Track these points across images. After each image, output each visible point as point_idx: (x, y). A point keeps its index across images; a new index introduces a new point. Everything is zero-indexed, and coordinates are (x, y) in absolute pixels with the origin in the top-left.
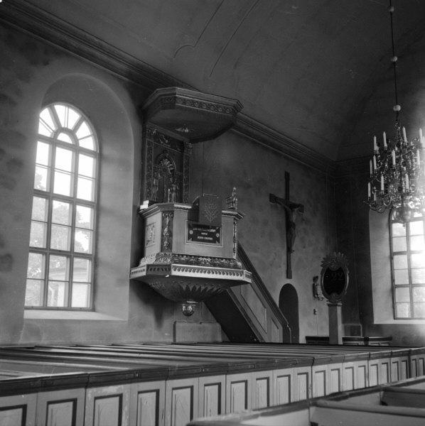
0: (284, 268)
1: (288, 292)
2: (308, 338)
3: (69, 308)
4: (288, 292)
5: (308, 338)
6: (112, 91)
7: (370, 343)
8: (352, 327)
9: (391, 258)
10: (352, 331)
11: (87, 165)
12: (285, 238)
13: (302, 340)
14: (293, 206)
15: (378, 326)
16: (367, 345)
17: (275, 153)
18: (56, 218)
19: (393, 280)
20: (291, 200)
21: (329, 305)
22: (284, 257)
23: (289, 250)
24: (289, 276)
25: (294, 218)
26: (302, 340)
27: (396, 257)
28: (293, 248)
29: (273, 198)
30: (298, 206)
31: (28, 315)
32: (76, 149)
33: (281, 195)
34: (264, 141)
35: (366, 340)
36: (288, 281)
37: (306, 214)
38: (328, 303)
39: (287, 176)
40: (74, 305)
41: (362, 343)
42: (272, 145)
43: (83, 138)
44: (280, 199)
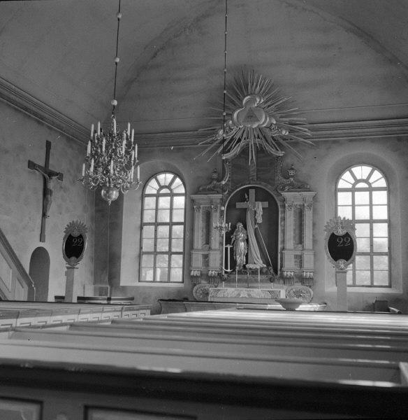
0: (38, 232)
1: (40, 256)
2: (56, 297)
3: (154, 281)
4: (40, 256)
5: (56, 297)
6: (375, 154)
7: (112, 302)
8: (100, 288)
9: (141, 228)
10: (102, 292)
11: (381, 198)
12: (41, 204)
13: (51, 298)
14: (51, 174)
15: (123, 287)
16: (108, 304)
17: (39, 122)
18: (148, 205)
19: (141, 248)
20: (51, 168)
21: (68, 268)
22: (39, 221)
23: (44, 215)
24: (42, 239)
25: (51, 185)
26: (51, 298)
27: (145, 228)
28: (49, 213)
29: (31, 165)
30: (57, 174)
31: (349, 290)
32: (371, 189)
33: (42, 163)
34: (26, 109)
35: (109, 299)
36: (41, 245)
37: (65, 182)
38: (67, 265)
39: (48, 145)
40: (375, 284)
41: (105, 302)
42: (36, 114)
43: (378, 180)
44: (39, 166)
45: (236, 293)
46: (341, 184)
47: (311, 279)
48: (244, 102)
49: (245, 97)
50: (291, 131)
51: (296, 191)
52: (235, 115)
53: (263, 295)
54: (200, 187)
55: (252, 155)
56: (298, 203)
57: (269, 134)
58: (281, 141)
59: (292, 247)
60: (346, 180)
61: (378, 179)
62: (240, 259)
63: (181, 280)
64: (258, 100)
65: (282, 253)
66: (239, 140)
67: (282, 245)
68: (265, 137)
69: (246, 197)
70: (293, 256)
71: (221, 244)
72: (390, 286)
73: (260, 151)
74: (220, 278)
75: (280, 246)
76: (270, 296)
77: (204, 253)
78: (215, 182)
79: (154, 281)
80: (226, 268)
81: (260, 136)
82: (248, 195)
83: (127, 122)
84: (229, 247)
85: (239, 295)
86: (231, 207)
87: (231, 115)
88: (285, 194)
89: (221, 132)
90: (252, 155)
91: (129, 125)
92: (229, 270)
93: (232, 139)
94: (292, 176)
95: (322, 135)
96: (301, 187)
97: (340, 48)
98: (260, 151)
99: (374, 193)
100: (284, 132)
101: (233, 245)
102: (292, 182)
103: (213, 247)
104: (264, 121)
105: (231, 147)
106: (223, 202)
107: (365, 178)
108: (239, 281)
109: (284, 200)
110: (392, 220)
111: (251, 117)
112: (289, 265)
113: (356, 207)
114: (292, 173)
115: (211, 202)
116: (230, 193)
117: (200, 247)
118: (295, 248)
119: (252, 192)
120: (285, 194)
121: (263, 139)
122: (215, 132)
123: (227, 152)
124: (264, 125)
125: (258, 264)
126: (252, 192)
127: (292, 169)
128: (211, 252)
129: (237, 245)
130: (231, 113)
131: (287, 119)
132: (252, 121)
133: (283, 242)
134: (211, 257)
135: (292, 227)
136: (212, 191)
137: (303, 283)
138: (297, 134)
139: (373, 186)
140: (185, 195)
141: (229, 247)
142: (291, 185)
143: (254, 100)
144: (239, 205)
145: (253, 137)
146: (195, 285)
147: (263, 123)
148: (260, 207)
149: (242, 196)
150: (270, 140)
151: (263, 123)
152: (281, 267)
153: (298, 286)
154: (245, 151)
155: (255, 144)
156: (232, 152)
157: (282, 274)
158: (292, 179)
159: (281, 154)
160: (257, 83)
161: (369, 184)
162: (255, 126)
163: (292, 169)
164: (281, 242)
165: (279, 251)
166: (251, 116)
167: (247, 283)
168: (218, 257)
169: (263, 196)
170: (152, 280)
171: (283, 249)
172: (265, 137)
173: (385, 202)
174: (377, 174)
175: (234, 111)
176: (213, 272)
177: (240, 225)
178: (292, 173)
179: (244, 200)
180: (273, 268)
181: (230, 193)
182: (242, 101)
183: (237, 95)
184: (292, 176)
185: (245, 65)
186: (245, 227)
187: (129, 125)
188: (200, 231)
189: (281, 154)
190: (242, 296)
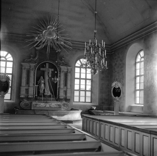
11: (10, 65)
32: (6, 61)
40: (86, 101)
45: (45, 105)
46: (77, 65)
47: (69, 100)
48: (48, 27)
49: (48, 25)
50: (65, 43)
51: (27, 63)
52: (44, 32)
53: (55, 106)
54: (25, 60)
55: (48, 50)
56: (66, 70)
57: (56, 42)
58: (60, 45)
59: (63, 87)
60: (78, 64)
61: (10, 57)
62: (41, 91)
63: (90, 101)
64: (54, 28)
65: (59, 89)
66: (44, 43)
67: (59, 87)
68: (54, 43)
69: (45, 66)
70: (63, 91)
71: (34, 84)
72: (91, 102)
73: (52, 48)
74: (36, 99)
75: (58, 87)
76: (58, 107)
77: (26, 88)
78: (32, 58)
79: (79, 102)
80: (36, 94)
81: (53, 42)
82: (46, 66)
83: (89, 40)
84: (37, 86)
85: (46, 106)
86: (39, 69)
87: (42, 32)
88: (62, 67)
89: (37, 38)
90: (48, 50)
91: (102, 41)
92: (36, 96)
93: (41, 42)
94: (63, 60)
95: (76, 46)
96: (67, 65)
97: (85, 15)
98: (52, 48)
99: (8, 63)
100: (62, 43)
101: (39, 85)
102: (63, 62)
103: (30, 86)
104: (54, 36)
105: (40, 45)
106: (35, 67)
107: (4, 56)
108: (44, 100)
109: (60, 69)
110: (93, 79)
111: (50, 34)
112: (62, 95)
113: (7, 68)
114: (63, 59)
115: (30, 66)
116: (38, 64)
117: (24, 85)
118: (63, 88)
119: (47, 64)
120: (62, 67)
121: (54, 44)
122: (34, 37)
123: (38, 47)
124: (55, 38)
125: (48, 93)
126: (47, 64)
127: (63, 57)
128: (30, 88)
129: (41, 85)
130: (41, 31)
131: (64, 38)
132: (49, 36)
133: (59, 85)
134: (30, 90)
135: (63, 80)
136: (30, 62)
137: (66, 101)
138: (66, 44)
139: (8, 60)
140: (75, 67)
141: (37, 86)
142: (63, 63)
143: (52, 28)
144: (42, 69)
145: (49, 42)
146: (21, 102)
147: (55, 38)
148: (51, 70)
149: (43, 66)
150: (56, 44)
151: (55, 38)
152: (58, 95)
153: (64, 102)
154: (45, 47)
155: (50, 45)
156: (40, 47)
157: (59, 98)
158: (63, 61)
159: (60, 50)
160: (54, 21)
161: (6, 59)
162: (51, 38)
163: (63, 57)
164: (59, 85)
165: (58, 89)
166: (50, 34)
167: (46, 101)
168: (33, 90)
169: (51, 66)
170: (84, 101)
171: (59, 88)
172: (54, 43)
173: (12, 66)
174: (9, 55)
175: (43, 30)
176: (31, 96)
177: (42, 77)
178: (63, 59)
179: (44, 67)
180: (55, 95)
181: (38, 64)
182: (47, 27)
183: (45, 24)
184: (63, 60)
185: (49, 12)
186: (44, 78)
187: (102, 41)
188: (25, 78)
189: (60, 50)
190: (47, 106)
